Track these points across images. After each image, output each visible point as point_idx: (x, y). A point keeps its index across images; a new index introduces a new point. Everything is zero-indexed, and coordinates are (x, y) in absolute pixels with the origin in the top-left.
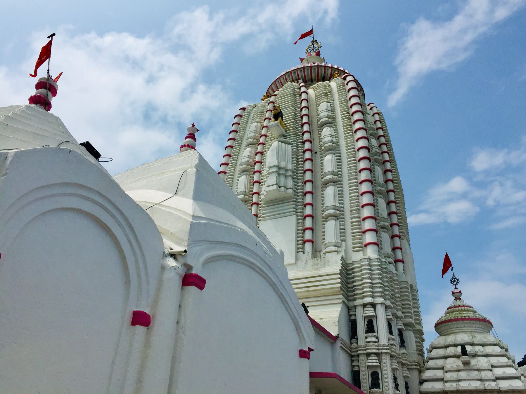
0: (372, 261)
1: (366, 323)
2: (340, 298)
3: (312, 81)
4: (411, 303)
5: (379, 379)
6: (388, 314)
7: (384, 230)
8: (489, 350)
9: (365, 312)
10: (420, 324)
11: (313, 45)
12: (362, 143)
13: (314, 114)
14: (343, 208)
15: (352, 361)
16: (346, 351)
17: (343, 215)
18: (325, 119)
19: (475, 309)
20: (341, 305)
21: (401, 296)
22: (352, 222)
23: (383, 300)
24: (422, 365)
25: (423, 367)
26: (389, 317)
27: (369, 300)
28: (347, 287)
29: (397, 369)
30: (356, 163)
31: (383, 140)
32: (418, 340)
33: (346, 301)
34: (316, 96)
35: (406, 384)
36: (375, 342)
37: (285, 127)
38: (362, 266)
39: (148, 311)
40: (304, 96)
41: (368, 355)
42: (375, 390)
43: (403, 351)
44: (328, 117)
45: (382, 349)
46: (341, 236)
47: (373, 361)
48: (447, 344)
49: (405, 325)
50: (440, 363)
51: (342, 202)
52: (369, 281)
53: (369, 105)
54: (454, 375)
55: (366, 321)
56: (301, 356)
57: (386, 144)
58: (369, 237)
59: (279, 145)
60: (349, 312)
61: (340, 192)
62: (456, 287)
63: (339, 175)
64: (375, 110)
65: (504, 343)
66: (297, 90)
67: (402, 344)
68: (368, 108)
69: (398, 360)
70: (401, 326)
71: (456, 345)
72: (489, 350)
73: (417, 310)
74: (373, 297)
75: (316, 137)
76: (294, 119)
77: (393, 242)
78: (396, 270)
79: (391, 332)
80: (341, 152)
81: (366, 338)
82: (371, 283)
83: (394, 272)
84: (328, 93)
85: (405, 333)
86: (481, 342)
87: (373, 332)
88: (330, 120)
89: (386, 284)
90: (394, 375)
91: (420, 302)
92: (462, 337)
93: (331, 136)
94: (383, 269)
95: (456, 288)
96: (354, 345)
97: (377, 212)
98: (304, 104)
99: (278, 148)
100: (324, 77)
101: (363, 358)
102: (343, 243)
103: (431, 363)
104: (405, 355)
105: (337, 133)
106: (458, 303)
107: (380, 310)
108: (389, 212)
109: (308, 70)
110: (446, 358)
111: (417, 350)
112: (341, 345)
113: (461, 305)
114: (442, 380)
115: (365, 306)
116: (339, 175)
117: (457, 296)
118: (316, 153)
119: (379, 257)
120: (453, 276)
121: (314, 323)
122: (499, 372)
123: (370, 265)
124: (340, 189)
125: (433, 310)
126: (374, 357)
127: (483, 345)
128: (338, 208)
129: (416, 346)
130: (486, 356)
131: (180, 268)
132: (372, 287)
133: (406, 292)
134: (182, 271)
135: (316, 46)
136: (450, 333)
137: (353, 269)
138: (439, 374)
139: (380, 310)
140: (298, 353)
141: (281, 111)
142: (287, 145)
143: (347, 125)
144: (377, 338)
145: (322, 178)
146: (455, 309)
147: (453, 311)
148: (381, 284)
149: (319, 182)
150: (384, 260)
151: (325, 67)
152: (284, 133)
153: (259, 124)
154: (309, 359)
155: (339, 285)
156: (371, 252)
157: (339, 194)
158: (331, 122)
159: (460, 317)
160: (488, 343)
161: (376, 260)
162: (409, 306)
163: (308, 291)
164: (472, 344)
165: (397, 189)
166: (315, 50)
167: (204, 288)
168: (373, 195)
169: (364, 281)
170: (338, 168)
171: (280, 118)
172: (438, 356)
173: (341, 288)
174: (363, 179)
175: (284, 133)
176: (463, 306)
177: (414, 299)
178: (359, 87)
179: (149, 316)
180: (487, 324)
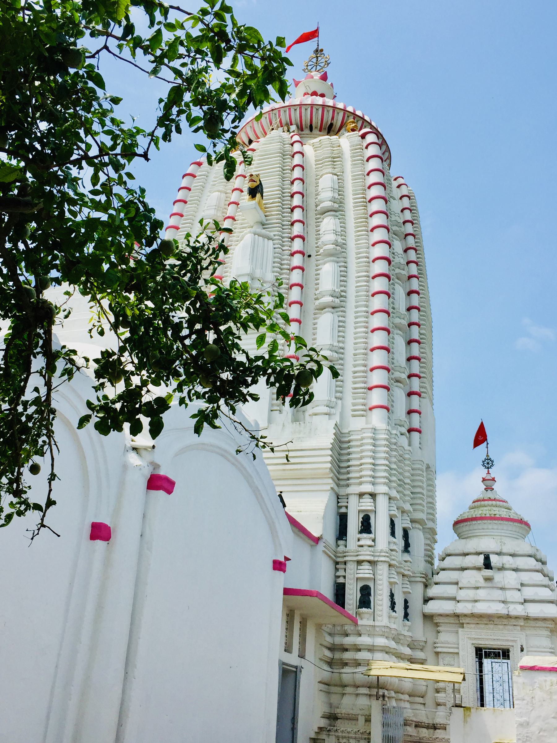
0: (377, 432)
1: (361, 520)
2: (329, 483)
3: (311, 129)
4: (425, 492)
5: (370, 594)
6: (392, 508)
7: (399, 384)
8: (521, 562)
9: (360, 504)
10: (433, 521)
11: (317, 57)
12: (380, 250)
13: (311, 189)
14: (343, 349)
15: (337, 570)
16: (330, 557)
17: (342, 359)
18: (328, 204)
19: (511, 504)
20: (328, 494)
21: (412, 481)
22: (355, 372)
23: (387, 488)
24: (430, 576)
25: (430, 579)
26: (392, 512)
27: (367, 488)
28: (339, 467)
29: (396, 583)
30: (368, 282)
31: (411, 241)
32: (429, 542)
33: (336, 488)
34: (316, 161)
35: (406, 602)
36: (370, 546)
37: (264, 208)
38: (362, 439)
39: (107, 522)
40: (297, 159)
41: (359, 563)
42: (364, 610)
43: (406, 557)
44: (334, 200)
45: (379, 556)
46: (337, 392)
47: (365, 571)
48: (466, 551)
49: (412, 521)
50: (453, 576)
51: (342, 338)
52: (371, 461)
53: (395, 179)
54: (471, 594)
55: (361, 515)
56: (275, 569)
57: (417, 263)
58: (377, 397)
59: (255, 239)
60: (338, 502)
61: (341, 324)
62: (488, 471)
63: (342, 296)
64: (404, 190)
65: (541, 554)
66: (288, 147)
67: (407, 548)
68: (395, 184)
69: (398, 570)
70: (408, 524)
71: (479, 554)
72: (521, 562)
73: (431, 511)
74: (374, 484)
75: (312, 229)
76: (280, 198)
77: (408, 349)
78: (410, 445)
79: (393, 534)
80: (348, 260)
81: (359, 540)
82: (374, 464)
83: (407, 447)
84: (335, 159)
85: (410, 533)
86: (512, 552)
87: (370, 532)
88: (336, 205)
89: (394, 466)
90: (391, 590)
91: (437, 489)
92: (487, 544)
93: (336, 232)
94: (391, 445)
95: (488, 473)
96: (342, 548)
97: (392, 360)
98: (297, 173)
99: (254, 243)
100: (331, 125)
101: (352, 567)
102: (339, 402)
103: (442, 576)
104: (408, 564)
105: (344, 228)
106: (489, 494)
107: (382, 501)
108: (409, 356)
109: (306, 109)
110: (463, 569)
111: (426, 555)
112: (324, 549)
113: (493, 498)
114: (454, 599)
115: (361, 495)
116: (342, 296)
117: (489, 483)
118: (309, 256)
119: (389, 428)
120: (487, 456)
121: (293, 522)
122: (529, 593)
123: (374, 439)
124: (341, 319)
125: (453, 495)
126: (366, 566)
127: (513, 555)
128: (336, 349)
129: (425, 550)
130: (516, 570)
131: (146, 467)
132: (374, 470)
133: (419, 475)
134: (147, 473)
135: (322, 60)
136: (473, 536)
137: (349, 442)
138: (451, 590)
139: (382, 501)
140: (271, 565)
141: (261, 184)
142: (266, 239)
143: (361, 218)
144: (374, 540)
145: (317, 299)
146: (483, 503)
147: (481, 506)
148: (387, 466)
149: (311, 306)
150: (394, 432)
151: (334, 108)
152: (264, 219)
153: (223, 195)
154: (284, 571)
155: (329, 465)
156: (378, 419)
157: (339, 326)
158: (337, 210)
159: (488, 515)
160: (521, 552)
161: (384, 432)
162: (421, 496)
163: (284, 470)
164: (499, 554)
165: (424, 320)
166: (318, 68)
167: (172, 492)
168: (389, 332)
169: (363, 461)
170: (341, 286)
171: (258, 195)
172: (445, 595)
173: (330, 469)
174: (376, 308)
175: (264, 219)
176: (495, 500)
177: (429, 485)
178: (382, 143)
179: (110, 527)
180: (523, 526)
